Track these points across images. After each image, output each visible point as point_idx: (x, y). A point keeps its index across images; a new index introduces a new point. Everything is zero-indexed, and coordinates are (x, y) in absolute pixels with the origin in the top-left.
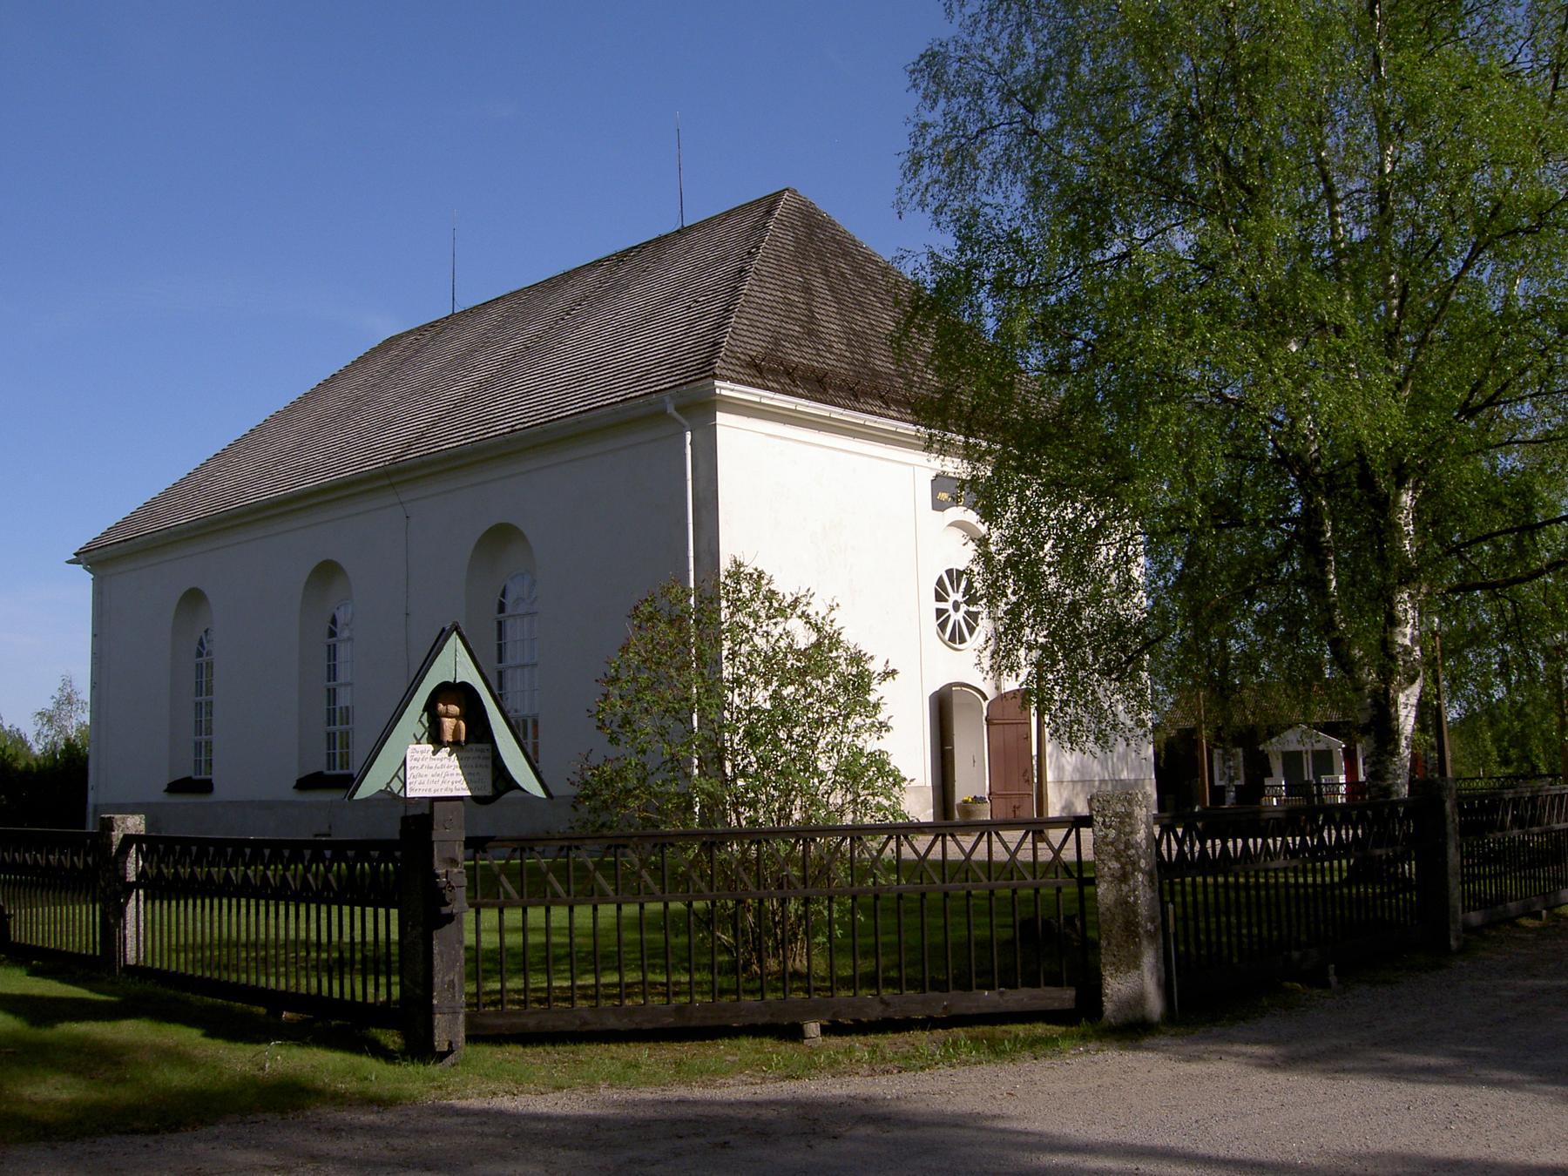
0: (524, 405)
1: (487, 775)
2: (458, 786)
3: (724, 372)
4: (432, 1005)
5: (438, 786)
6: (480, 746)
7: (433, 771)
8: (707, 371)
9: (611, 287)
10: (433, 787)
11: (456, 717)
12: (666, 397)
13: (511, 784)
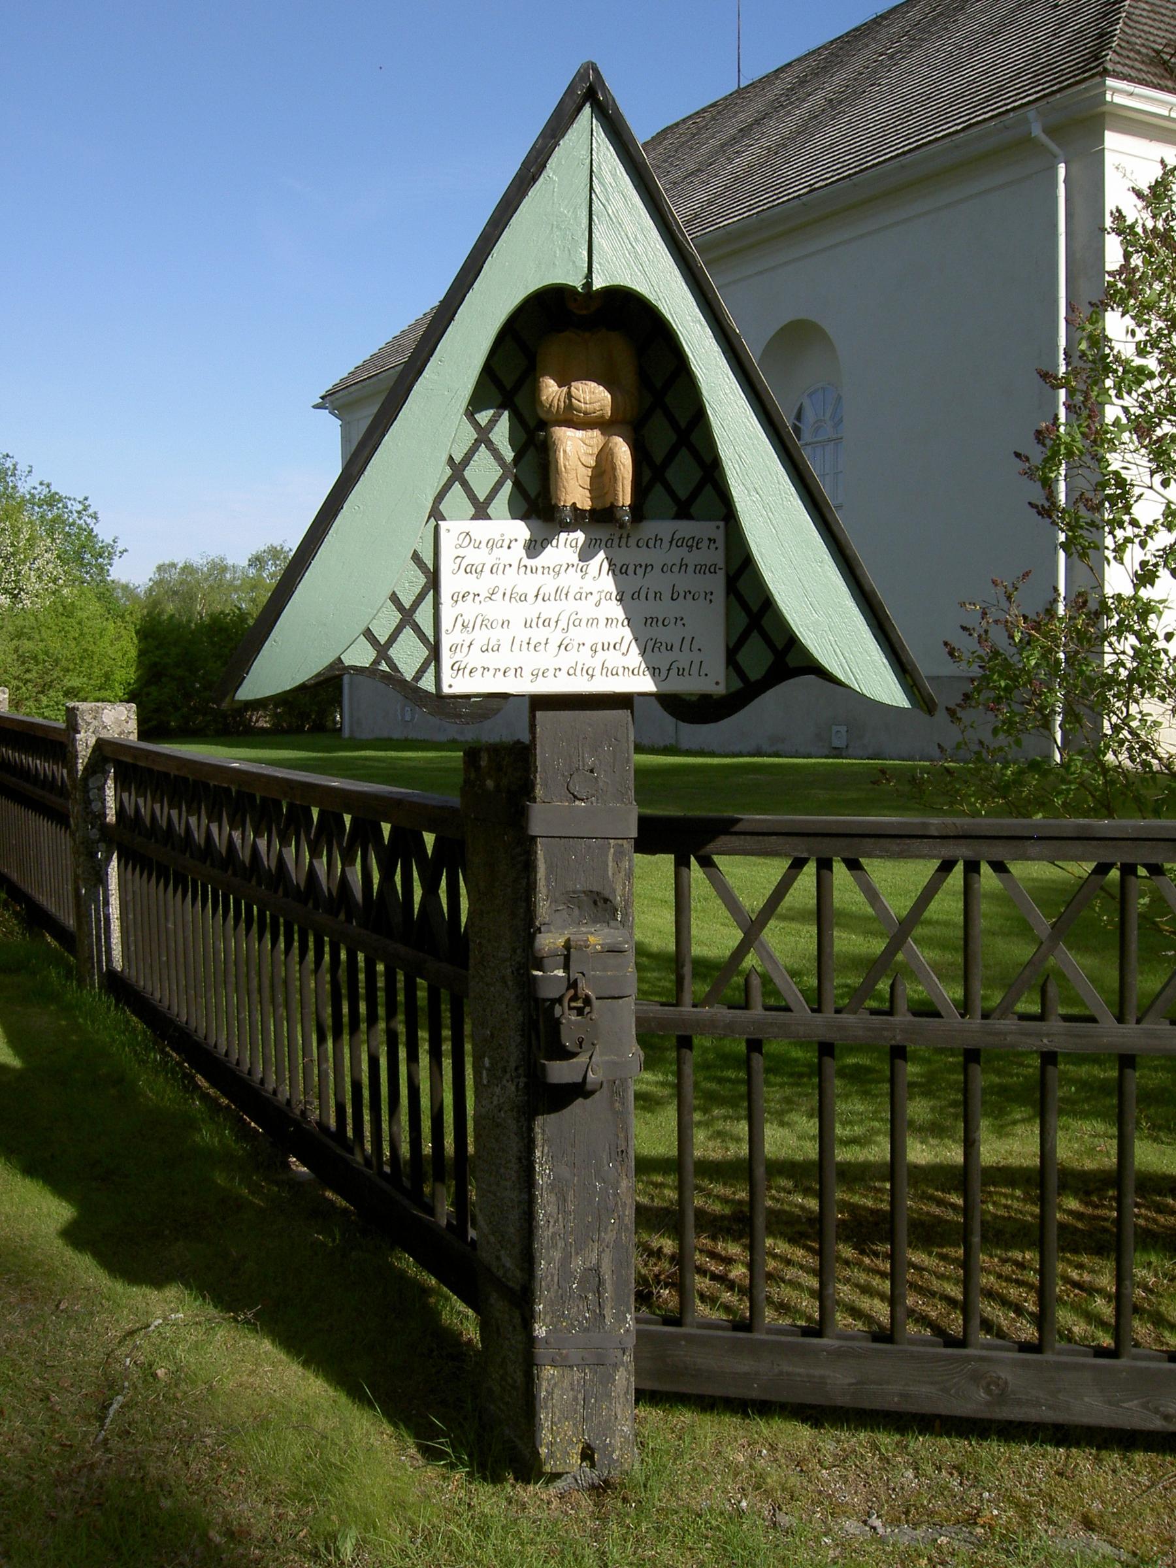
0: (827, 159)
1: (709, 625)
2: (614, 659)
3: (1119, 68)
4: (532, 1311)
5: (545, 659)
6: (686, 528)
7: (530, 610)
8: (1093, 66)
9: (941, 14)
10: (530, 661)
11: (605, 426)
12: (1031, 113)
13: (788, 659)
